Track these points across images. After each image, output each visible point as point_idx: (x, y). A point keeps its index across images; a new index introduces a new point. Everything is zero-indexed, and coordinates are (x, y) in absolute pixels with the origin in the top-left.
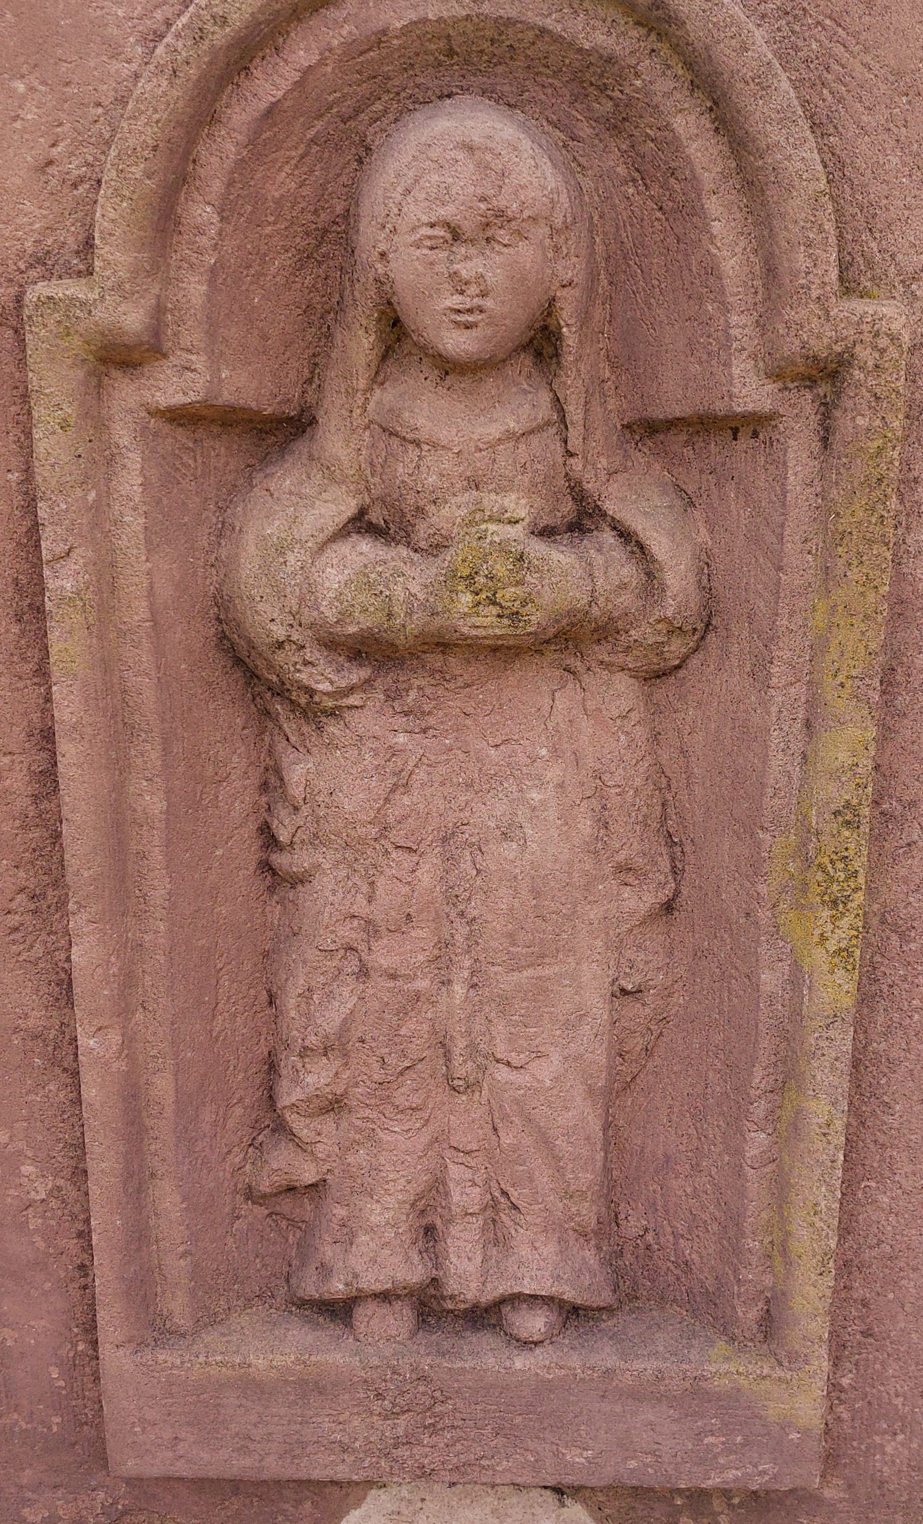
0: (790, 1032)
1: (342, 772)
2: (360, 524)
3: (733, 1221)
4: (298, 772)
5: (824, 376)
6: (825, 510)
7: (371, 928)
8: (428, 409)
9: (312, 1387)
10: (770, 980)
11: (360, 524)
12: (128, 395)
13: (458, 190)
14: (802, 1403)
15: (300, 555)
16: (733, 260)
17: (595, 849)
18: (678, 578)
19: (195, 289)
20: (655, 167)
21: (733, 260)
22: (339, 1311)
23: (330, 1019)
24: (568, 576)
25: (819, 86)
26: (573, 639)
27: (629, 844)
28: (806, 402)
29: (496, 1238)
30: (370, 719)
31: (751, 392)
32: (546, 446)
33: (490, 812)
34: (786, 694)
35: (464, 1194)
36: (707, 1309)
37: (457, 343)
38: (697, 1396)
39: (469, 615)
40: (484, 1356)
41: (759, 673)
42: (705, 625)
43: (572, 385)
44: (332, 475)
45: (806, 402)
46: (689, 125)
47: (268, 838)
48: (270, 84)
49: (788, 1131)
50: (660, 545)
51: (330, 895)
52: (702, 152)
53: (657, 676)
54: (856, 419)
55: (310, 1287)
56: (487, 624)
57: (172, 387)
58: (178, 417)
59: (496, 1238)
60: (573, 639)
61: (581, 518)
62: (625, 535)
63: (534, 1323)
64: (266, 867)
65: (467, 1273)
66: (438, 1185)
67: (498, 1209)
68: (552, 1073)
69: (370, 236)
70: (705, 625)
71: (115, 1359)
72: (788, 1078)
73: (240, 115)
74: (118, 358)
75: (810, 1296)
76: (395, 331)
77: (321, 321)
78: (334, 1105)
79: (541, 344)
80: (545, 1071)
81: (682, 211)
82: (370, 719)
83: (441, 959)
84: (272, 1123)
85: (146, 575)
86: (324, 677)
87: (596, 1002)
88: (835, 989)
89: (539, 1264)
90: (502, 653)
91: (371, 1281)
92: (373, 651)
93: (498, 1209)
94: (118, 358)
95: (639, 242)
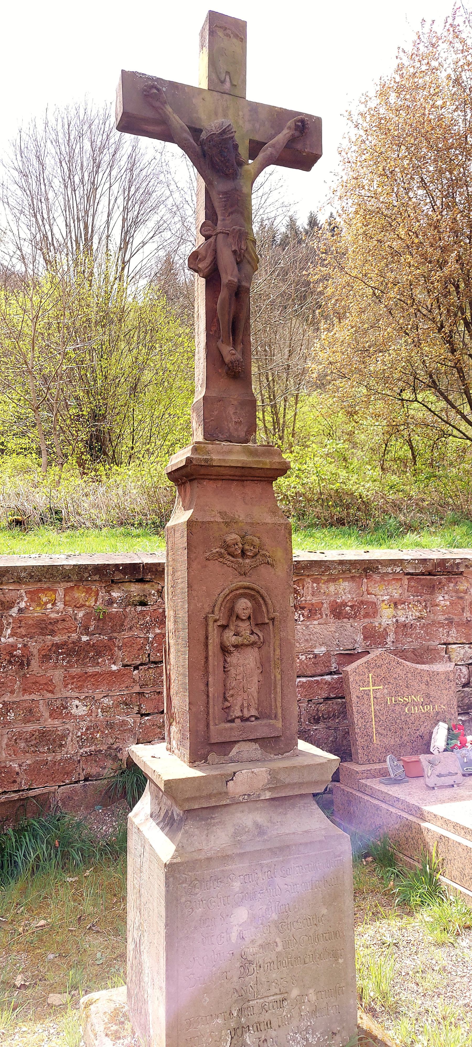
0: (275, 683)
1: (234, 659)
2: (234, 635)
3: (271, 706)
4: (228, 660)
5: (273, 619)
6: (274, 630)
7: (236, 675)
8: (241, 624)
9: (232, 729)
10: (273, 677)
11: (234, 635)
12: (216, 624)
13: (244, 606)
14: (279, 724)
15: (230, 638)
16: (265, 610)
17: (256, 665)
18: (262, 638)
19: (222, 615)
20: (257, 603)
21: (265, 610)
22: (232, 721)
23: (233, 685)
24: (253, 638)
25: (405, 902)
26: (253, 644)
27: (259, 665)
28: (271, 622)
29: (249, 710)
30: (235, 653)
31: (267, 621)
32: (250, 626)
33: (247, 662)
34: (272, 648)
35: (245, 705)
36: (269, 717)
37: (244, 618)
38: (270, 725)
39: (246, 642)
40: (248, 723)
41: (269, 646)
42: (263, 643)
43: (251, 621)
44: (232, 630)
45: (271, 622)
46: (260, 599)
47: (224, 667)
48: (228, 598)
49: (276, 693)
50: (260, 635)
51: (233, 672)
52: (262, 602)
53: (259, 648)
54: (276, 623)
55: (230, 718)
56: (247, 643)
57: (219, 623)
58: (219, 626)
59: (249, 710)
60: (253, 644)
61: (252, 633)
62: (257, 634)
63: (253, 719)
64: (224, 671)
65: (246, 714)
66: (243, 704)
67: (249, 706)
68: (253, 689)
69: (236, 609)
70: (263, 643)
71: (212, 727)
72: (275, 688)
73: (226, 600)
74: (216, 621)
75: (280, 715)
76: (238, 617)
77: (230, 616)
78: (232, 696)
79: (249, 618)
80: (253, 689)
81: (260, 606)
82: (235, 653)
83: (243, 678)
84: (225, 699)
85: (217, 640)
86: (232, 649)
87: (257, 682)
88: (279, 677)
89: (253, 712)
90: (247, 646)
91: (237, 715)
92: (236, 646)
93: (249, 706)
94: (216, 621)
95: (257, 608)
